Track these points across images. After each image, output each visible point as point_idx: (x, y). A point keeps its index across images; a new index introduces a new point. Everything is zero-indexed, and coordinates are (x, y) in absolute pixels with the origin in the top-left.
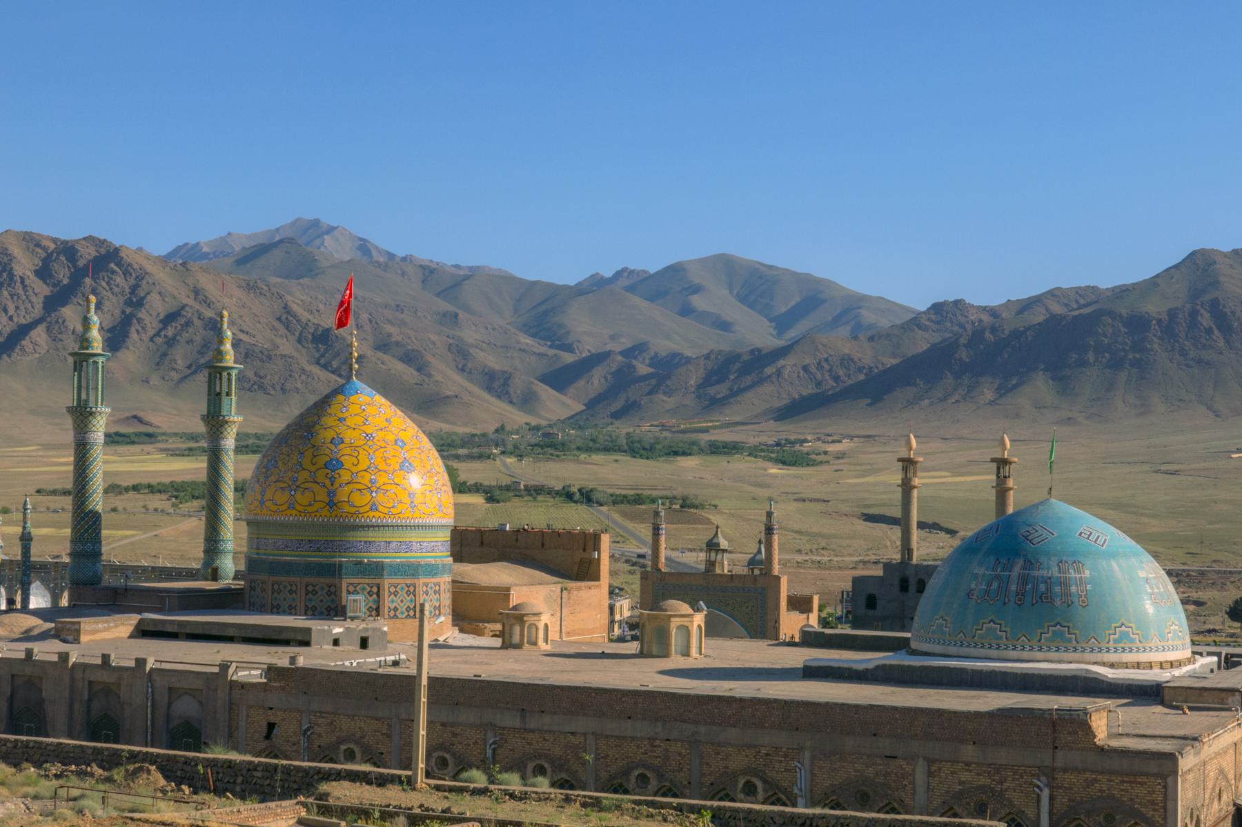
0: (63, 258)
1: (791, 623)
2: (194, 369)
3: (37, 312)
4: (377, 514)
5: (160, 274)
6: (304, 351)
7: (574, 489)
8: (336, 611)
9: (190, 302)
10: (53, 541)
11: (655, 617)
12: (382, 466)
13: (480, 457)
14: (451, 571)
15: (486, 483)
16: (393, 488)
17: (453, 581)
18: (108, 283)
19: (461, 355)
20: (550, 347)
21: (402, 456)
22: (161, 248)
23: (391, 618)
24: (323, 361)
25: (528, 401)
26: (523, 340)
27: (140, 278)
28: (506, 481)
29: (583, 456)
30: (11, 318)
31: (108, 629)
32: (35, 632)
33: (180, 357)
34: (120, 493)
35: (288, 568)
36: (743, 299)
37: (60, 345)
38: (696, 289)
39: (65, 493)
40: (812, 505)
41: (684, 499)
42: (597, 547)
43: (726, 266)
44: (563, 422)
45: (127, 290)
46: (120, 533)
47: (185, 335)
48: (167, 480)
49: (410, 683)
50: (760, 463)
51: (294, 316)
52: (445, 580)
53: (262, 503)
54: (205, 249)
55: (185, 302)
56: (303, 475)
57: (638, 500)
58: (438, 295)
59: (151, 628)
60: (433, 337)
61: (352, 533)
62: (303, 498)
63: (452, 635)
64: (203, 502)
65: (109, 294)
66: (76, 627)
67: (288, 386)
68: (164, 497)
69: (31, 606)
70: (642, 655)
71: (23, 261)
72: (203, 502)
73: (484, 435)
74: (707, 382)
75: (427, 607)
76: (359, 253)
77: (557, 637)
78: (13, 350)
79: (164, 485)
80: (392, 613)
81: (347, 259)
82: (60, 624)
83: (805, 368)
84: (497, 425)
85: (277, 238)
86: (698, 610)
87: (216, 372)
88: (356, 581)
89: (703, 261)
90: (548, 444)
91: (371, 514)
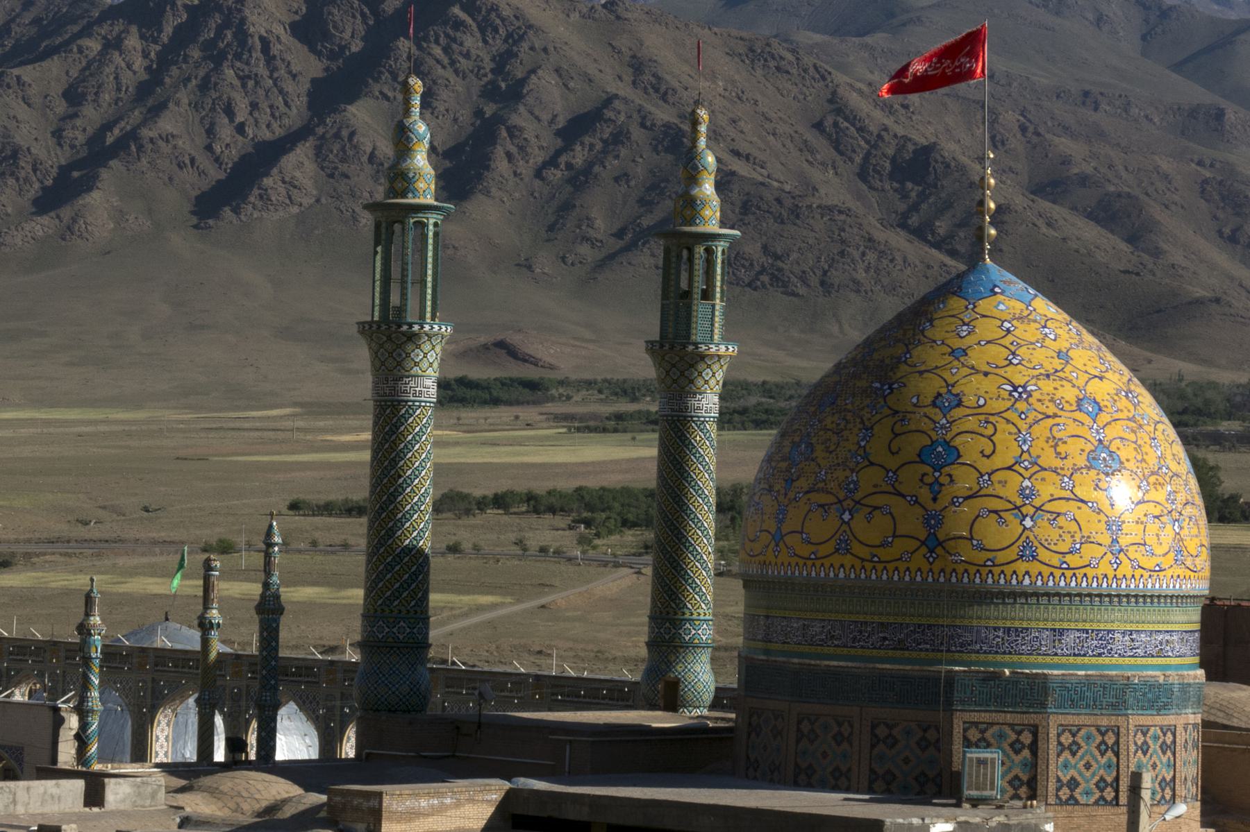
2: (630, 238)
4: (1035, 568)
9: (624, 89)
10: (328, 613)
12: (1048, 459)
14: (1200, 701)
17: (1206, 724)
18: (446, 50)
21: (1092, 436)
23: (1062, 803)
24: (914, 220)
27: (514, 38)
30: (240, 129)
31: (441, 810)
33: (600, 213)
34: (468, 512)
39: (352, 510)
45: (488, 65)
46: (466, 599)
47: (612, 164)
48: (567, 485)
51: (853, 119)
53: (778, 538)
55: (612, 89)
56: (870, 478)
58: (1178, 67)
59: (532, 812)
60: (1165, 165)
61: (992, 611)
62: (869, 530)
64: (649, 535)
65: (449, 74)
66: (373, 803)
67: (836, 276)
68: (561, 521)
69: (281, 755)
72: (649, 535)
75: (1147, 781)
78: (244, 198)
79: (562, 495)
80: (1065, 793)
87: (681, 244)
88: (985, 717)
91: (1022, 567)
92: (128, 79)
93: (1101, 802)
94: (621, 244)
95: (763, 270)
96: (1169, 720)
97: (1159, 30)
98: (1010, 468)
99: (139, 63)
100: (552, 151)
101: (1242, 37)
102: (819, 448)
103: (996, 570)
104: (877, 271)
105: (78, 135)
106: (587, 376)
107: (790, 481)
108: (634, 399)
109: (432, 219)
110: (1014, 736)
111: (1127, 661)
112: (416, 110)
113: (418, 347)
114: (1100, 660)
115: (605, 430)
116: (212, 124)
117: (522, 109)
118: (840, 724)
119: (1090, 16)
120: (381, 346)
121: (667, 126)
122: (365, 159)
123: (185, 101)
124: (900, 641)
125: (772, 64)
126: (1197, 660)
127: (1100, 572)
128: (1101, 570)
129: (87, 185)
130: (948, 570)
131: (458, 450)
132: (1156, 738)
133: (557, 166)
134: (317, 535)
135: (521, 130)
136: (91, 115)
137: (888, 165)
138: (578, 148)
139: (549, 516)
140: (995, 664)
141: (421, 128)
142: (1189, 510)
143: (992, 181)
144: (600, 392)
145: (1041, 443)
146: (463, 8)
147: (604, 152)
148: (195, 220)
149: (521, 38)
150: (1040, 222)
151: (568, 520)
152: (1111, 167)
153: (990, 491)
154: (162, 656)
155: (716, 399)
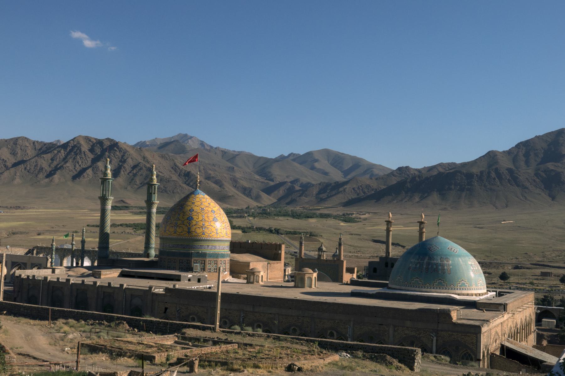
1: (347, 277)
2: (142, 184)
3: (89, 163)
5: (132, 152)
7: (273, 229)
8: (189, 269)
9: (142, 161)
10: (93, 243)
11: (300, 274)
13: (241, 217)
14: (229, 256)
16: (210, 227)
22: (132, 141)
25: (257, 198)
27: (125, 153)
28: (249, 225)
29: (276, 218)
30: (80, 166)
32: (86, 274)
33: (138, 180)
35: (174, 254)
36: (332, 164)
37: (96, 175)
38: (316, 161)
39: (97, 226)
40: (355, 236)
41: (311, 233)
42: (280, 249)
43: (327, 153)
48: (132, 223)
49: (215, 294)
50: (337, 221)
51: (178, 167)
53: (165, 231)
54: (148, 143)
56: (179, 222)
57: (295, 233)
58: (227, 161)
60: (225, 175)
62: (179, 230)
63: (229, 278)
64: (145, 231)
67: (175, 191)
68: (131, 228)
70: (295, 287)
73: (242, 209)
74: (319, 193)
75: (221, 268)
77: (266, 280)
82: (94, 272)
83: (353, 189)
84: (247, 206)
85: (173, 140)
86: (315, 272)
87: (150, 185)
89: (319, 151)
90: (264, 213)
92: (62, 157)
93: (214, 272)
99: (63, 155)
105: (53, 166)
109: (111, 181)
128: (215, 237)
129: (54, 174)
136: (55, 163)
141: (109, 166)
154: (65, 249)
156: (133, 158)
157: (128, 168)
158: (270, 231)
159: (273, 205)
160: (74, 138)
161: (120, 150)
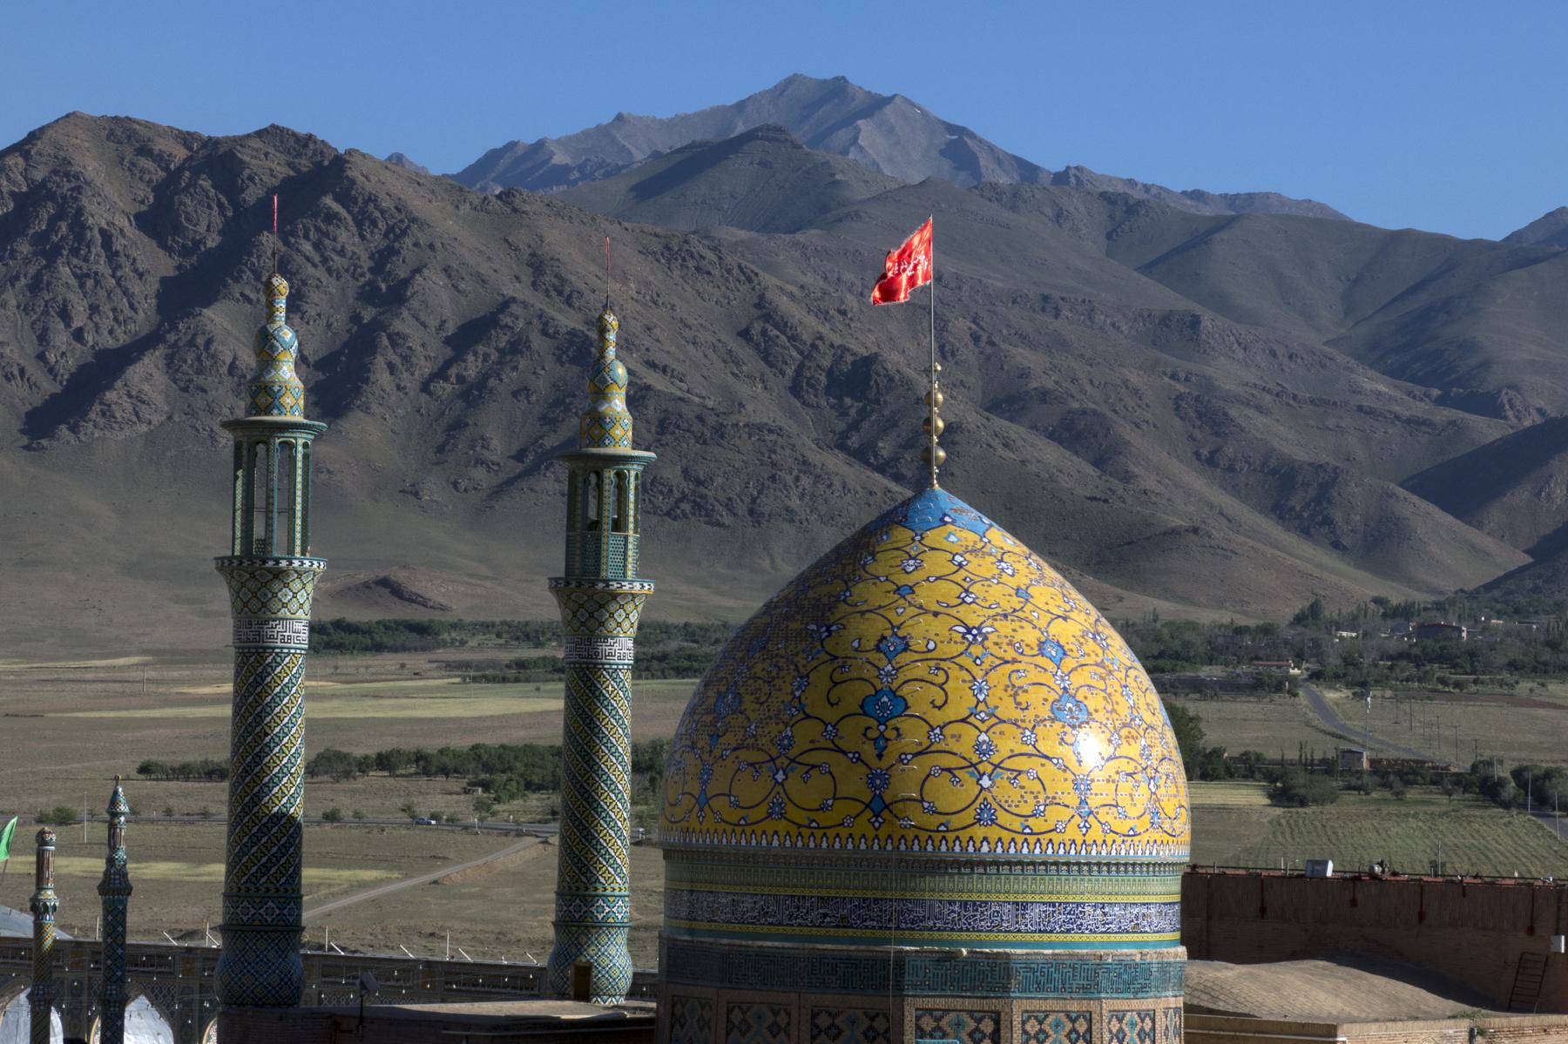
0: (206, 183)
2: (530, 460)
3: (144, 317)
4: (994, 833)
5: (445, 221)
6: (807, 415)
7: (1503, 772)
9: (521, 291)
12: (1007, 710)
13: (1257, 686)
14: (1182, 982)
15: (1272, 754)
17: (1189, 1008)
18: (317, 246)
19: (1206, 423)
20: (1439, 402)
21: (1057, 685)
22: (446, 152)
24: (854, 441)
25: (1379, 544)
26: (1367, 385)
27: (396, 233)
28: (1324, 749)
29: (1524, 686)
30: (78, 335)
33: (497, 432)
34: (348, 775)
37: (199, 402)
39: (212, 773)
44: (1472, 595)
45: (366, 264)
47: (510, 376)
48: (462, 743)
51: (783, 326)
52: (1167, 1003)
53: (703, 801)
54: (560, 158)
55: (509, 291)
56: (807, 732)
58: (1147, 269)
60: (1134, 378)
61: (990, 884)
62: (805, 792)
64: (556, 799)
65: (320, 273)
67: (767, 504)
68: (455, 784)
71: (109, 190)
72: (556, 799)
73: (1266, 630)
76: (946, 164)
78: (84, 415)
79: (456, 755)
81: (917, 178)
85: (740, 128)
87: (589, 469)
88: (941, 1003)
90: (1432, 655)
91: (979, 832)
94: (520, 467)
95: (684, 498)
96: (1147, 1004)
97: (1126, 227)
98: (964, 720)
100: (440, 362)
101: (1219, 235)
102: (747, 698)
103: (951, 836)
104: (813, 496)
106: (484, 617)
107: (715, 737)
108: (538, 645)
109: (301, 439)
110: (973, 1025)
111: (1099, 937)
112: (281, 314)
113: (287, 585)
114: (1069, 937)
115: (504, 680)
116: (45, 330)
117: (405, 314)
118: (775, 1014)
119: (1048, 211)
120: (243, 585)
121: (572, 333)
122: (224, 370)
123: (13, 302)
124: (843, 918)
125: (691, 263)
126: (1177, 935)
127: (1066, 837)
128: (1067, 834)
130: (896, 837)
131: (335, 703)
132: (1133, 1024)
133: (446, 379)
134: (172, 802)
135: (405, 337)
137: (823, 378)
138: (471, 358)
139: (441, 779)
140: (952, 943)
141: (288, 335)
142: (1165, 767)
143: (940, 397)
144: (499, 635)
145: (999, 691)
146: (336, 199)
147: (500, 363)
148: (25, 440)
149: (404, 232)
150: (996, 443)
151: (464, 783)
152: (1074, 380)
153: (942, 746)
155: (630, 644)
156: (461, 268)
157: (426, 348)
158: (1483, 787)
159: (1500, 592)
160: (33, 136)
161: (364, 211)
